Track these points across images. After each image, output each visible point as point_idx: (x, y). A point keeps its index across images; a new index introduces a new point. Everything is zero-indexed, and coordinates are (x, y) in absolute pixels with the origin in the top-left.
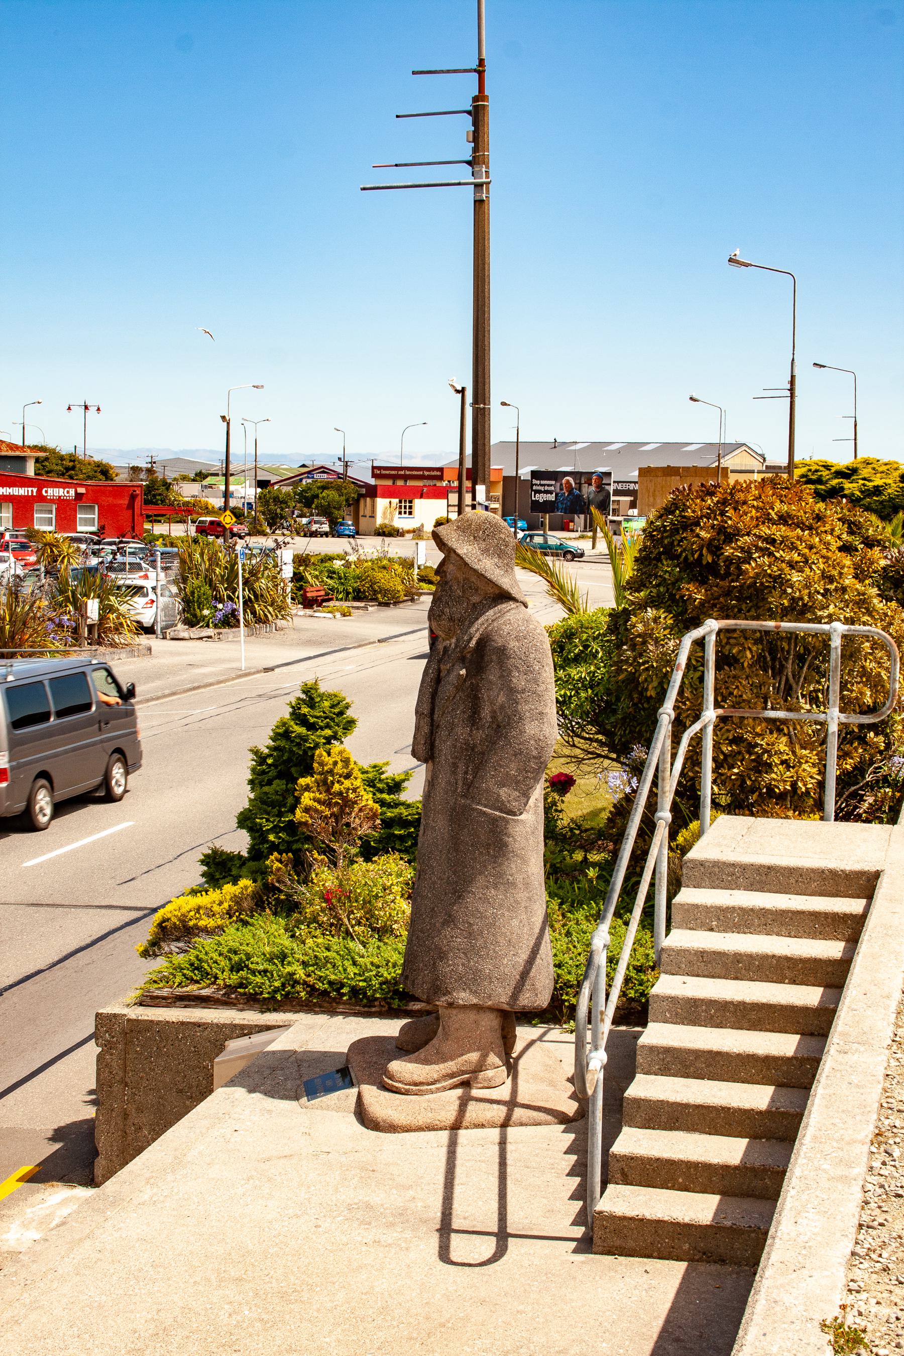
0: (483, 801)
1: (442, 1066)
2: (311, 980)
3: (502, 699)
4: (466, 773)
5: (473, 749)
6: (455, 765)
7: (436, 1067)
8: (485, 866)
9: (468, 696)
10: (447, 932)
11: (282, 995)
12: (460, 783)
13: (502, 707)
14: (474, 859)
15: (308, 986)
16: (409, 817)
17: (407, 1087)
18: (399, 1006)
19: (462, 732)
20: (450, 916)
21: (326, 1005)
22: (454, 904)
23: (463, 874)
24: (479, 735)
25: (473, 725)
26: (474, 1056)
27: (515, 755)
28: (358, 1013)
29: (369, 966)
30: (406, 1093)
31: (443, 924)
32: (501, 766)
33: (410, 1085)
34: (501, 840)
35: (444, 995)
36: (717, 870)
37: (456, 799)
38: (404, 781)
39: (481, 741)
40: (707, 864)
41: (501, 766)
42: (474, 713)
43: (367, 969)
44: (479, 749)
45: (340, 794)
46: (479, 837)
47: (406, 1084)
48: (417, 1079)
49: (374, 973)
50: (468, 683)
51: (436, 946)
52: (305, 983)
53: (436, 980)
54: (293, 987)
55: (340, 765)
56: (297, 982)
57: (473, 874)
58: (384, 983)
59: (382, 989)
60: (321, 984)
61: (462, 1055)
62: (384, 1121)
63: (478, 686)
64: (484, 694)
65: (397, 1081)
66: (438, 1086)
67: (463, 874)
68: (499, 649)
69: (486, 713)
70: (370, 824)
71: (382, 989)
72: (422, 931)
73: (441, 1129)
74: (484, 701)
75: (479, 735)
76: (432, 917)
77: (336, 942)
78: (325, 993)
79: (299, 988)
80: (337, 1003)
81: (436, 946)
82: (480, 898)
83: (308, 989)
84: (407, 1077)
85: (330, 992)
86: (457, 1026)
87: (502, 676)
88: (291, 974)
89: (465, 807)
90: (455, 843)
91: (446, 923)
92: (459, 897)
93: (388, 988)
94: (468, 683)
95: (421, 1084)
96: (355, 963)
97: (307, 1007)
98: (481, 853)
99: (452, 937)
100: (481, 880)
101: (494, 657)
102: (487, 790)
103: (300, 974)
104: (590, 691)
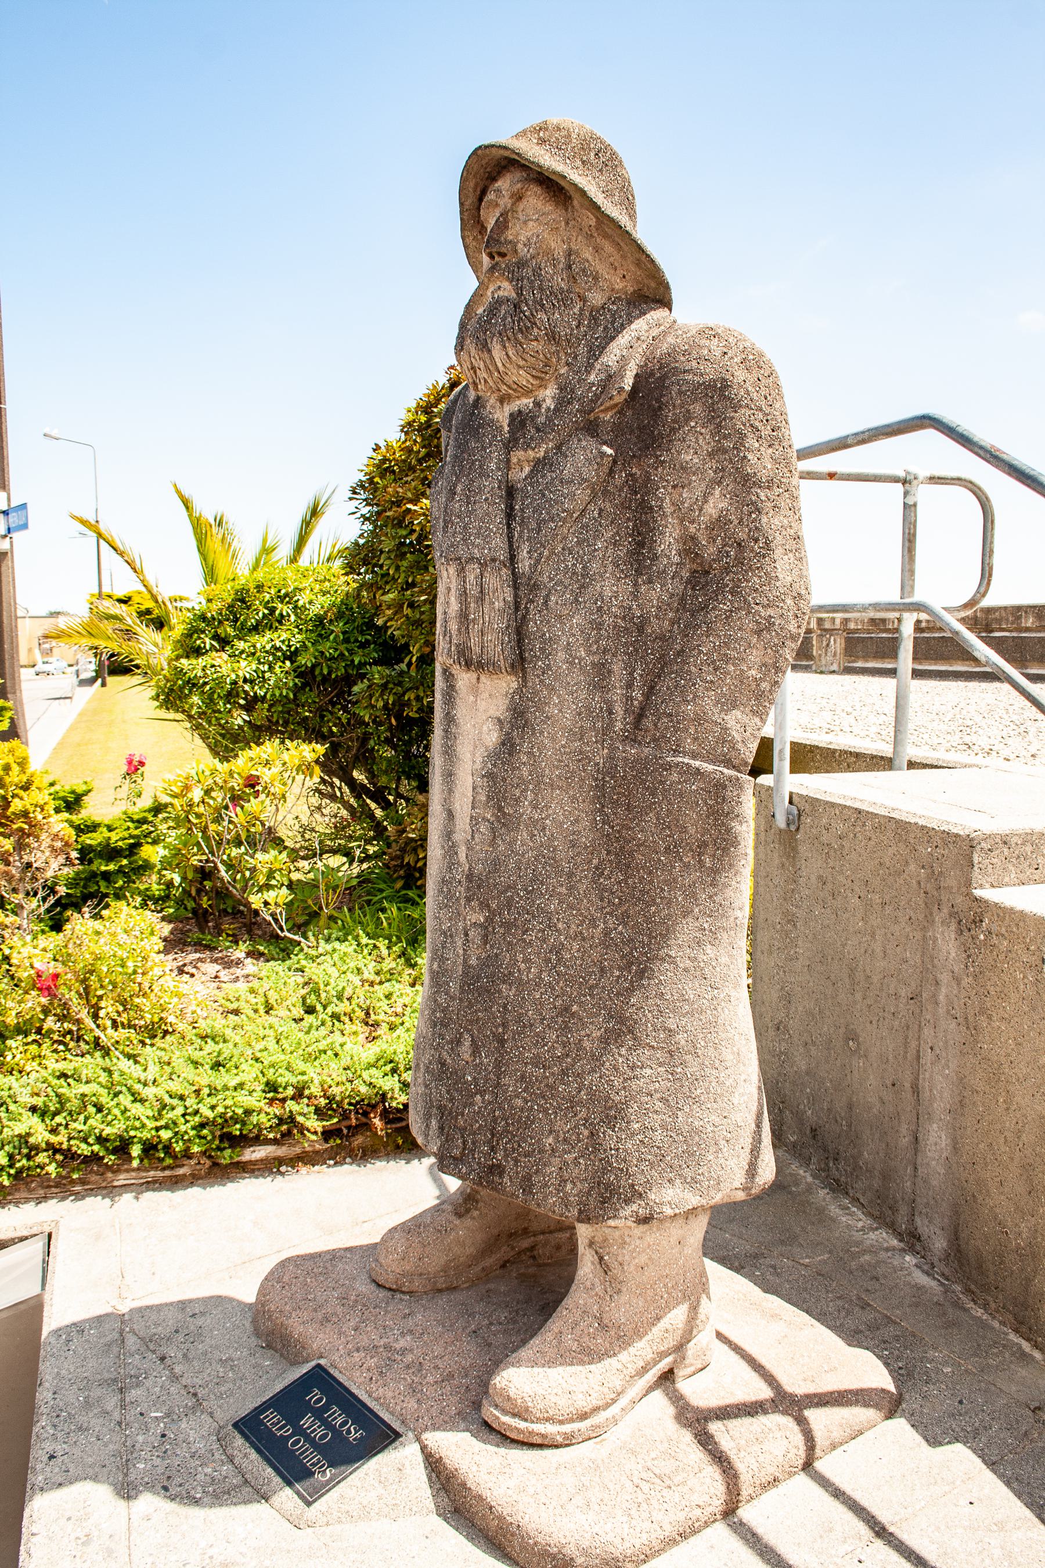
0: (689, 744)
1: (623, 1356)
2: (60, 1139)
3: (716, 504)
4: (629, 686)
5: (641, 629)
6: (602, 670)
7: (611, 1363)
8: (694, 895)
9: (624, 506)
10: (620, 1056)
11: (9, 1175)
12: (619, 710)
13: (720, 523)
14: (672, 883)
15: (56, 1151)
16: (120, 843)
17: (567, 1428)
18: (231, 1158)
19: (611, 587)
20: (622, 1020)
21: (94, 1178)
22: (631, 990)
23: (648, 920)
24: (655, 594)
25: (639, 573)
26: (678, 1316)
27: (759, 633)
28: (155, 1182)
29: (167, 1100)
30: (567, 1442)
31: (605, 1041)
32: (727, 659)
33: (572, 1420)
34: (728, 831)
35: (628, 1201)
36: (1029, 848)
37: (613, 749)
38: (83, 795)
39: (659, 608)
40: (1014, 840)
41: (727, 659)
42: (641, 545)
43: (164, 1106)
44: (655, 626)
45: (25, 814)
46: (684, 830)
47: (561, 1422)
48: (583, 1403)
49: (180, 1111)
50: (620, 478)
51: (591, 1093)
52: (51, 1147)
53: (604, 1171)
54: (29, 1157)
55: (16, 769)
56: (35, 1149)
57: (669, 916)
58: (202, 1126)
59: (201, 1137)
60: (83, 1146)
61: (658, 1319)
62: (585, 1552)
63: (648, 479)
64: (665, 498)
65: (539, 1420)
66: (623, 1401)
67: (648, 920)
68: (710, 386)
69: (668, 542)
70: (61, 859)
71: (201, 1137)
72: (536, 1062)
73: (707, 1525)
74: (664, 516)
75: (655, 594)
76: (565, 1028)
77: (90, 1065)
78: (95, 1158)
79: (42, 1158)
80: (114, 1172)
81: (591, 1093)
82: (686, 970)
83: (59, 1157)
84: (564, 1405)
85: (103, 1158)
86: (643, 1259)
87: (718, 451)
88: (24, 1138)
89: (641, 766)
90: (618, 851)
91: (611, 1038)
92: (641, 974)
93: (212, 1133)
94: (620, 478)
95: (596, 1410)
96: (138, 1099)
97: (61, 1188)
98: (687, 866)
99: (633, 1068)
100: (686, 930)
101: (697, 408)
102: (699, 719)
103: (41, 1135)
104: (288, 663)
